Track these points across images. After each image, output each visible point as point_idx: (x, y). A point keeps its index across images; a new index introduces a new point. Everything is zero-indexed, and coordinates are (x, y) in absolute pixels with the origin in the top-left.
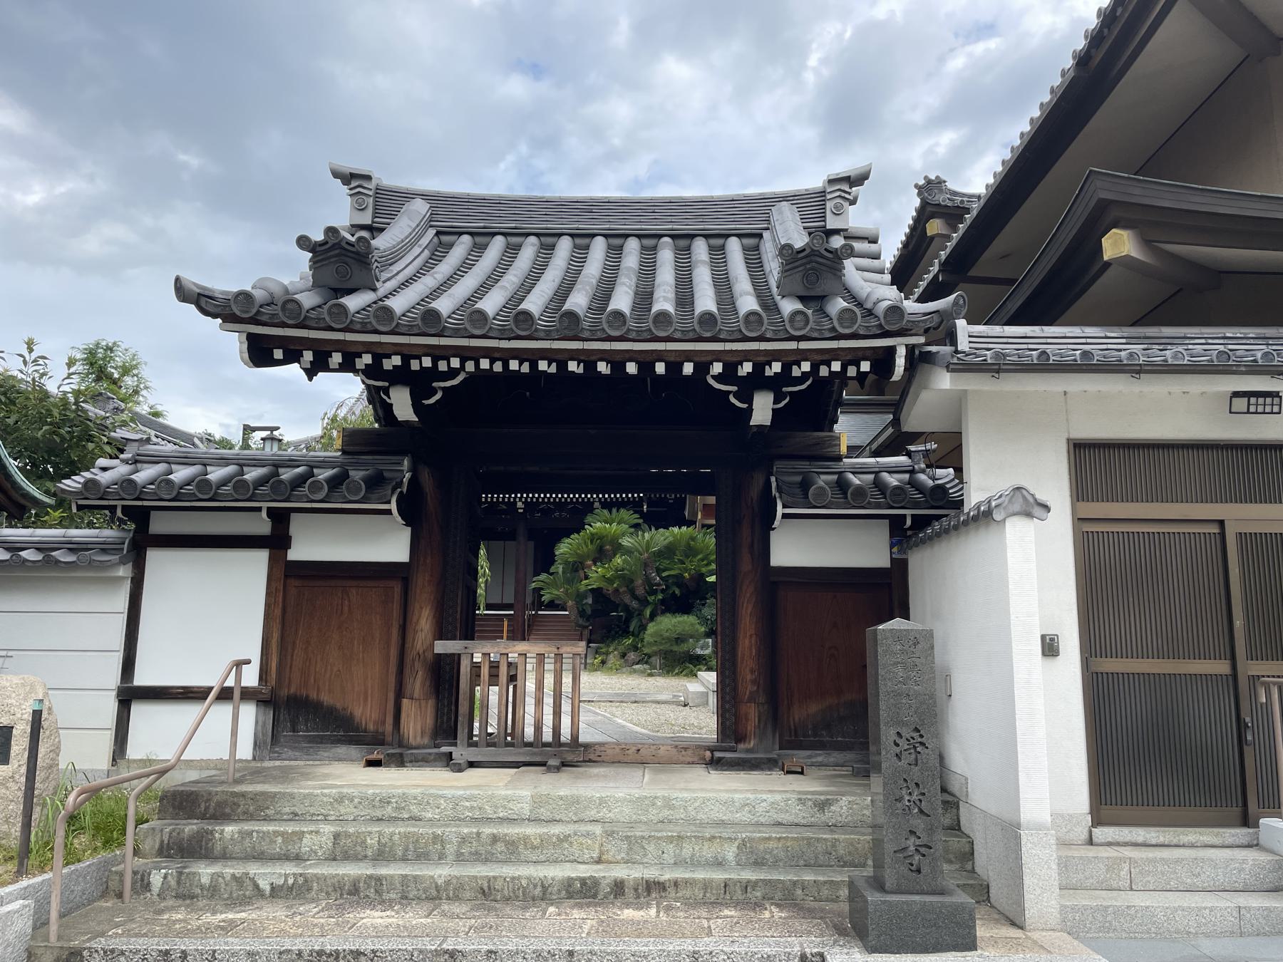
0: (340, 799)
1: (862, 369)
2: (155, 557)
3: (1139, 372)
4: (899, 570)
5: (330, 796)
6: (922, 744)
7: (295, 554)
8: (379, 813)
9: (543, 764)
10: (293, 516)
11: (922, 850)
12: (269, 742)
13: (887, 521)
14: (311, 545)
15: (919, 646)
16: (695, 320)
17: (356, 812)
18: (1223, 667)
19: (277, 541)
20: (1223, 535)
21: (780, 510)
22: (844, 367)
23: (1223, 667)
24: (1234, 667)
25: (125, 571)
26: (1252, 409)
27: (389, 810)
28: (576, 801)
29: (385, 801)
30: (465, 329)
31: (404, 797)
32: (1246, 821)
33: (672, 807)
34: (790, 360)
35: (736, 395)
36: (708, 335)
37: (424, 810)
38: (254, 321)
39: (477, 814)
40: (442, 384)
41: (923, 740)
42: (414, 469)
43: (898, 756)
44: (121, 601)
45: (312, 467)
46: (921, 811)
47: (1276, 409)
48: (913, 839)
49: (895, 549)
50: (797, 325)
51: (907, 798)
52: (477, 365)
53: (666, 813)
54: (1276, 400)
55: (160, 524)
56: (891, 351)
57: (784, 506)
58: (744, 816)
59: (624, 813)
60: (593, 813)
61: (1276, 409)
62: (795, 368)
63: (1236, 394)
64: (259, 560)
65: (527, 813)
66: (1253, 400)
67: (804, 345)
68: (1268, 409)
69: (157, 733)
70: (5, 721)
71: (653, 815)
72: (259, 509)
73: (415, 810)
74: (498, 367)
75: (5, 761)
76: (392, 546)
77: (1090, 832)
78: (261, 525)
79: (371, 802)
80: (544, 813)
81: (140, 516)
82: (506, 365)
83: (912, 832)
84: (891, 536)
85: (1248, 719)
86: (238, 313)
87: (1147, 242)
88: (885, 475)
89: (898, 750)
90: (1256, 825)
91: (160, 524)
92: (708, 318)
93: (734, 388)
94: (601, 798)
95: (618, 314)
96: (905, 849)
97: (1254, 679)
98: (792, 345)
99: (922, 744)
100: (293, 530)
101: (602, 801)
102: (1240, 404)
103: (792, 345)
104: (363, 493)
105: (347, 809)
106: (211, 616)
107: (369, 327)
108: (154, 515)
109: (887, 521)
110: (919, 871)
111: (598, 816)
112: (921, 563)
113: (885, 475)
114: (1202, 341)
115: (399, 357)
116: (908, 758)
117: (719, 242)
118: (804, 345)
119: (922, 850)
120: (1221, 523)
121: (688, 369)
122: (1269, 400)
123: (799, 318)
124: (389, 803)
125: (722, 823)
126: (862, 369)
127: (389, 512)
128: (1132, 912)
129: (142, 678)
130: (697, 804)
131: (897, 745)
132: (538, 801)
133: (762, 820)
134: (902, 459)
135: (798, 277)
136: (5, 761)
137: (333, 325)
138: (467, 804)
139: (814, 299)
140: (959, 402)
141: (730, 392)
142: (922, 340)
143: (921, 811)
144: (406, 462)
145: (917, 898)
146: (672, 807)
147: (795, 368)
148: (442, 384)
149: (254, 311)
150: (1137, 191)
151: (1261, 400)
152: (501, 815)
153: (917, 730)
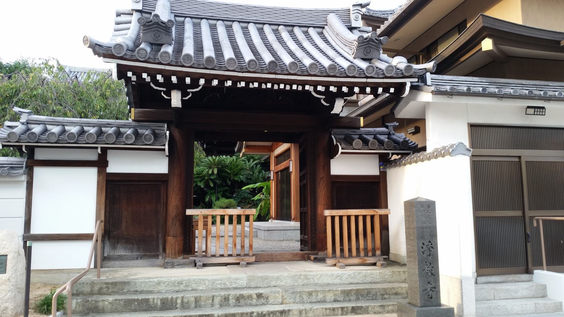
0: (159, 283)
1: (281, 87)
2: (38, 171)
3: (502, 98)
4: (383, 175)
5: (153, 282)
6: (432, 247)
7: (110, 170)
8: (177, 289)
9: (238, 264)
10: (109, 151)
11: (433, 289)
12: (102, 260)
13: (378, 156)
14: (119, 165)
15: (430, 208)
16: (204, 61)
17: (167, 289)
18: (519, 213)
19: (101, 163)
20: (520, 162)
21: (340, 150)
22: (273, 86)
23: (519, 213)
24: (524, 213)
25: (24, 178)
26: (536, 113)
27: (182, 287)
28: (267, 278)
29: (180, 283)
30: (225, 67)
31: (189, 281)
32: (528, 271)
33: (307, 279)
34: (195, 79)
35: (324, 100)
36: (332, 74)
37: (198, 286)
38: (121, 58)
39: (223, 286)
40: (192, 90)
41: (432, 246)
42: (168, 129)
43: (423, 253)
44: (22, 192)
45: (119, 128)
46: (432, 274)
47: (543, 113)
48: (429, 285)
49: (381, 167)
50: (369, 72)
51: (427, 269)
52: (291, 87)
53: (305, 281)
54: (544, 110)
55: (39, 155)
56: (404, 84)
57: (342, 149)
58: (337, 281)
59: (288, 282)
60: (273, 283)
61: (543, 113)
62: (251, 84)
63: (529, 107)
64: (93, 172)
65: (245, 285)
66: (536, 110)
67: (369, 80)
68: (541, 113)
69: (45, 256)
70: (2, 253)
71: (300, 282)
72: (97, 148)
73: (194, 286)
74: (300, 88)
75: (4, 272)
76: (158, 165)
77: (476, 279)
78: (93, 156)
79: (173, 284)
80: (253, 284)
81: (31, 150)
82: (304, 87)
83: (429, 283)
84: (380, 162)
85: (529, 233)
86: (115, 54)
87: (495, 44)
88: (378, 136)
89: (423, 250)
90: (532, 273)
91: (39, 155)
92: (209, 59)
93: (165, 89)
94: (277, 277)
95: (188, 56)
96: (426, 290)
97: (532, 218)
98: (364, 80)
99: (432, 247)
100: (109, 158)
101: (278, 278)
102: (531, 111)
103: (364, 80)
104: (152, 141)
105: (162, 288)
106: (70, 200)
107: (179, 64)
108: (36, 150)
109: (378, 156)
110: (431, 298)
111: (276, 284)
112: (393, 174)
113: (378, 136)
114: (513, 86)
115: (231, 82)
116: (427, 253)
117: (245, 25)
118: (369, 80)
119: (433, 289)
120: (520, 157)
121: (215, 82)
122: (541, 110)
123: (314, 66)
124: (182, 284)
125: (328, 284)
126: (281, 87)
127: (164, 150)
128: (499, 307)
129: (35, 230)
130: (318, 277)
131: (423, 248)
132: (250, 279)
133: (345, 282)
134: (384, 129)
135: (362, 50)
136: (4, 272)
137: (162, 62)
138: (218, 282)
139: (157, 46)
140: (425, 107)
141: (161, 91)
142: (416, 80)
143: (432, 274)
144: (166, 125)
145: (433, 308)
146: (307, 279)
147: (251, 84)
148: (192, 90)
149: (123, 53)
150: (497, 24)
151: (539, 110)
152: (234, 286)
153: (430, 242)
